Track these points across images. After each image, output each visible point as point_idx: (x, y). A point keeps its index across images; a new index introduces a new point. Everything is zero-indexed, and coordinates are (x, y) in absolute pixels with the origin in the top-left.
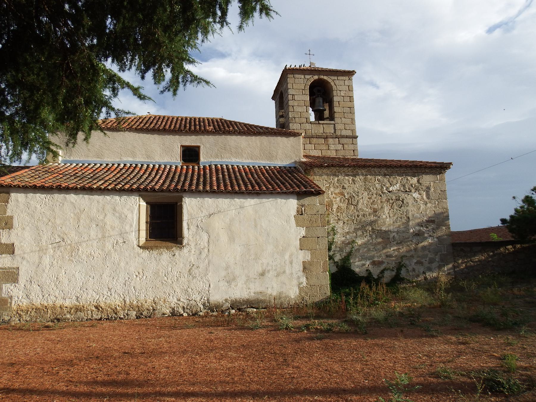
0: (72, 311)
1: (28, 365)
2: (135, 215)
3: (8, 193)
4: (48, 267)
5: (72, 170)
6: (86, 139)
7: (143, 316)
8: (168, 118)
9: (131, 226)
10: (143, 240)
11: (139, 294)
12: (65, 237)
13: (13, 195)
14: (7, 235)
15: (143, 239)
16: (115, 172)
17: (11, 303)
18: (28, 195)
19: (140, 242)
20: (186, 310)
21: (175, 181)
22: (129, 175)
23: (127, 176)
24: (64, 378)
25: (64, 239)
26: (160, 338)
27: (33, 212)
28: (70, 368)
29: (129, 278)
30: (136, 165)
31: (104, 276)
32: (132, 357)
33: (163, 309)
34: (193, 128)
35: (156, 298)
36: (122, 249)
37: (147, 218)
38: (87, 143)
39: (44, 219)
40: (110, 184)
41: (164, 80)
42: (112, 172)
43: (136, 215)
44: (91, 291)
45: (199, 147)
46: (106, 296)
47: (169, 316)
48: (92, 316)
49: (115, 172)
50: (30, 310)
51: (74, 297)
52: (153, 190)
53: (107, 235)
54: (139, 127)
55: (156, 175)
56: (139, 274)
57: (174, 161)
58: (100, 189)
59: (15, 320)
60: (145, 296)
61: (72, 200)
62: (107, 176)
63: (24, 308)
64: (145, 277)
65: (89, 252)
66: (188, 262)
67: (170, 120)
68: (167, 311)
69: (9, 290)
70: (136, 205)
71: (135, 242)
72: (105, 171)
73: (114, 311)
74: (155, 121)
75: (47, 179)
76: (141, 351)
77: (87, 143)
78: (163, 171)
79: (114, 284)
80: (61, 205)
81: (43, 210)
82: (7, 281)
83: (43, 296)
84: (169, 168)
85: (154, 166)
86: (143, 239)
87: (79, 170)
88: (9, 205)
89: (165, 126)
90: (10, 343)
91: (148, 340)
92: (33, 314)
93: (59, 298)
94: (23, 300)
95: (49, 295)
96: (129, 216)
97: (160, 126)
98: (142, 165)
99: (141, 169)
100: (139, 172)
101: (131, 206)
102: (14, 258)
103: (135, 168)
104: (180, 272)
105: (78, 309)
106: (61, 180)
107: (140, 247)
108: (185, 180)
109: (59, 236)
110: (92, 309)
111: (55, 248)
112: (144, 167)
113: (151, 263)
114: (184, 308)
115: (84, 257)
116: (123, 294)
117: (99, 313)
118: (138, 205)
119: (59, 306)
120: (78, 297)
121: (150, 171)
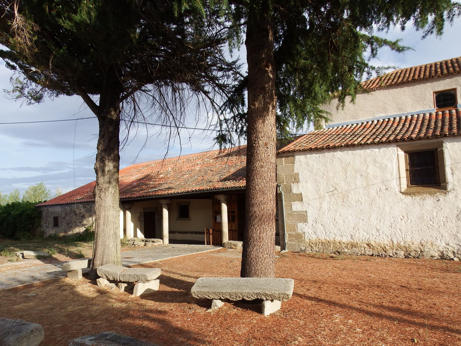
0: (349, 246)
1: (326, 283)
2: (394, 164)
3: (294, 156)
4: (327, 210)
5: (335, 132)
6: (352, 101)
7: (411, 256)
8: (421, 68)
9: (392, 174)
10: (404, 186)
11: (405, 236)
12: (337, 187)
13: (297, 157)
14: (296, 187)
15: (404, 186)
16: (371, 129)
17: (305, 237)
18: (307, 156)
19: (402, 189)
20: (457, 255)
21: (431, 127)
22: (383, 129)
23: (382, 130)
24: (356, 299)
25: (336, 188)
26: (434, 278)
27: (312, 168)
28: (358, 291)
29: (394, 221)
30: (389, 119)
31: (372, 219)
32: (410, 291)
33: (431, 252)
34: (445, 71)
35: (423, 241)
36: (386, 195)
37: (406, 166)
38: (354, 103)
39: (320, 173)
40: (368, 139)
41: (427, 22)
42: (368, 129)
43: (396, 164)
44: (362, 231)
45: (455, 90)
46: (375, 236)
47: (438, 259)
48: (365, 252)
49: (371, 129)
50: (318, 243)
51: (349, 235)
52: (410, 139)
53: (371, 183)
54: (388, 84)
55: (410, 125)
56: (404, 218)
57: (428, 109)
58: (361, 144)
59: (309, 250)
60: (412, 239)
61: (339, 157)
62: (364, 132)
63: (314, 242)
64: (409, 221)
65: (357, 198)
66: (455, 208)
67: (418, 70)
68: (436, 254)
69: (303, 228)
70: (395, 155)
71: (397, 189)
72: (362, 129)
73: (383, 249)
74: (402, 75)
75: (318, 142)
76: (417, 287)
77: (354, 103)
78: (417, 120)
79: (381, 225)
80: (331, 161)
81: (318, 167)
82: (300, 221)
83: (326, 233)
84: (422, 116)
85: (406, 117)
86: (404, 186)
87: (340, 131)
88: (295, 165)
89: (413, 77)
90: (310, 266)
91: (422, 278)
92: (320, 246)
93: (338, 235)
94: (312, 235)
95: (330, 233)
96: (389, 165)
97: (408, 78)
98: (395, 118)
99: (394, 122)
100: (392, 125)
101: (389, 156)
102: (303, 203)
103: (388, 122)
104: (446, 217)
105: (353, 246)
106: (328, 141)
107: (403, 193)
108: (443, 125)
109: (332, 186)
110: (365, 246)
111: (330, 195)
112: (397, 119)
113: (414, 208)
114: (454, 253)
115: (353, 202)
116: (390, 235)
117: (371, 250)
118: (396, 155)
119: (338, 242)
120: (352, 236)
121: (403, 122)
